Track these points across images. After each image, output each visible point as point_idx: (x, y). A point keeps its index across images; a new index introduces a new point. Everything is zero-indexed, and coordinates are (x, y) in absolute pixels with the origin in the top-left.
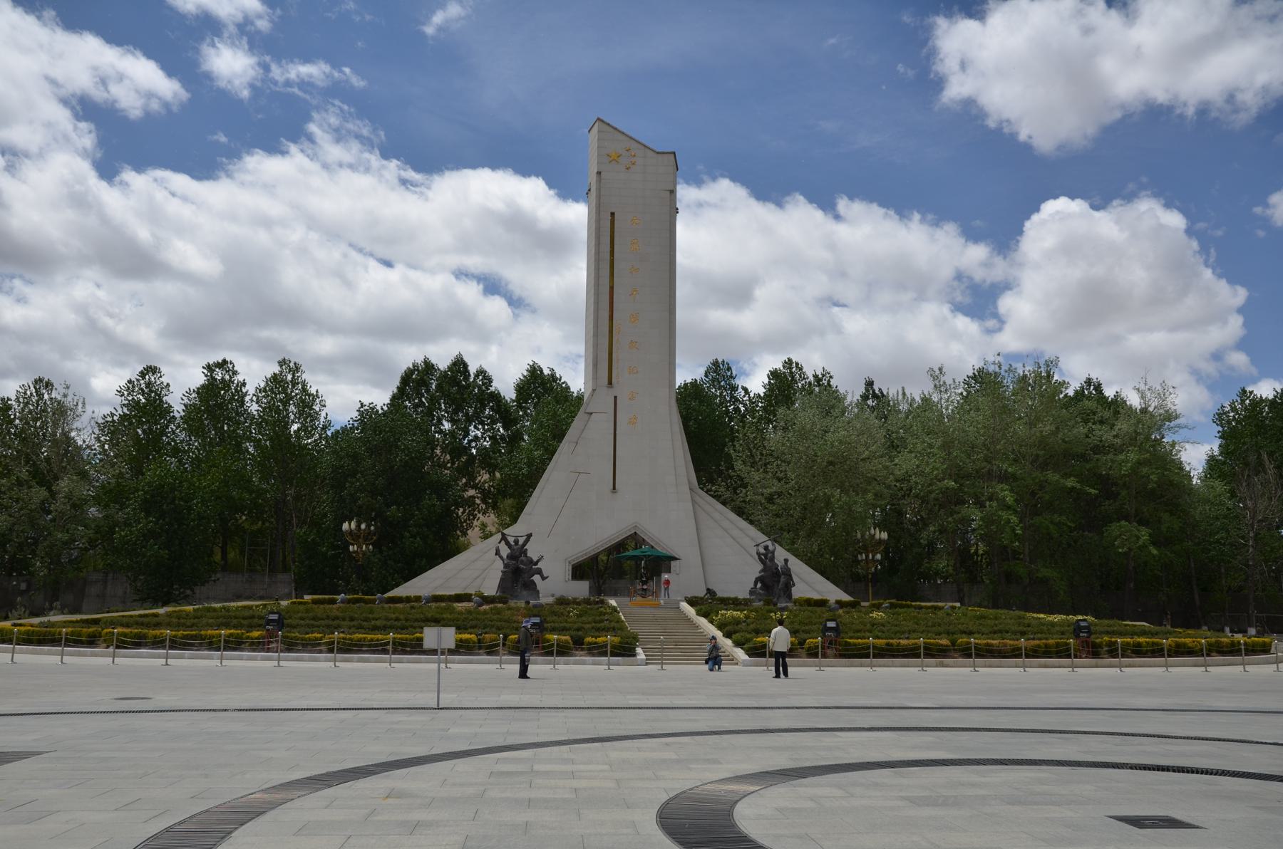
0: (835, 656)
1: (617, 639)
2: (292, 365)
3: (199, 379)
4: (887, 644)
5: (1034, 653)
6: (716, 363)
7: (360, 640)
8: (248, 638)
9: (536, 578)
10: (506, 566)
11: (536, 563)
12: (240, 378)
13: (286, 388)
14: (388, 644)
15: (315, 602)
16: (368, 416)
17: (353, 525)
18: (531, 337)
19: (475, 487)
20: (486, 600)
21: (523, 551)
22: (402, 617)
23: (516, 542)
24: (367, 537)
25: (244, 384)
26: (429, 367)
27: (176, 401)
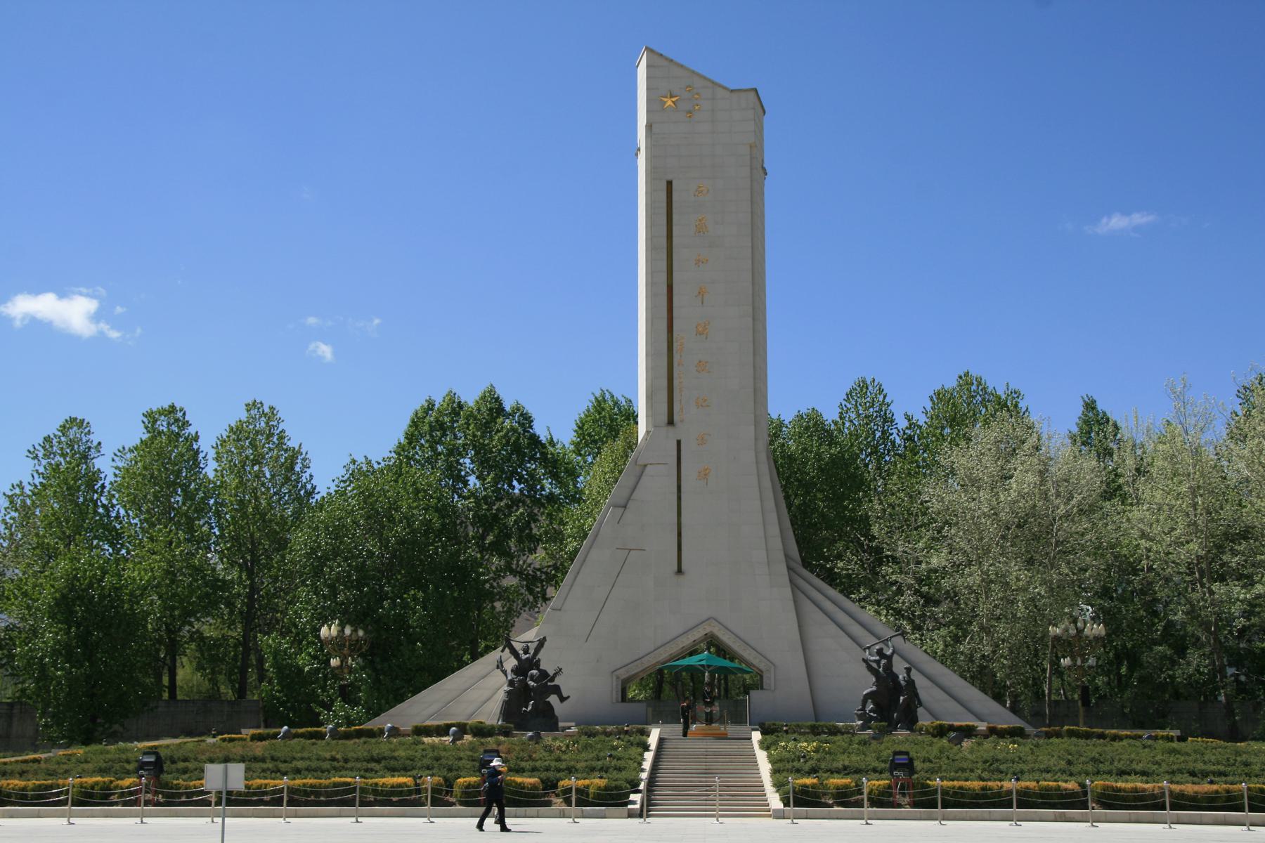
0: (915, 805)
1: (602, 783)
2: (267, 410)
3: (136, 434)
4: (983, 789)
5: (1184, 803)
6: (863, 386)
7: (260, 787)
8: (116, 787)
9: (553, 699)
10: (511, 683)
11: (552, 679)
12: (191, 430)
13: (257, 438)
14: (281, 791)
15: (254, 738)
16: (359, 474)
17: (334, 630)
18: (572, 355)
19: (514, 573)
20: (481, 731)
21: (533, 663)
22: (338, 756)
23: (526, 651)
24: (354, 647)
25: (196, 438)
26: (456, 408)
27: (107, 466)
